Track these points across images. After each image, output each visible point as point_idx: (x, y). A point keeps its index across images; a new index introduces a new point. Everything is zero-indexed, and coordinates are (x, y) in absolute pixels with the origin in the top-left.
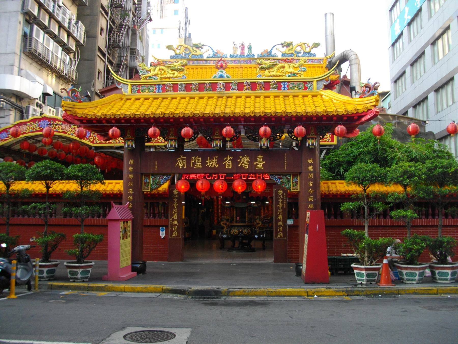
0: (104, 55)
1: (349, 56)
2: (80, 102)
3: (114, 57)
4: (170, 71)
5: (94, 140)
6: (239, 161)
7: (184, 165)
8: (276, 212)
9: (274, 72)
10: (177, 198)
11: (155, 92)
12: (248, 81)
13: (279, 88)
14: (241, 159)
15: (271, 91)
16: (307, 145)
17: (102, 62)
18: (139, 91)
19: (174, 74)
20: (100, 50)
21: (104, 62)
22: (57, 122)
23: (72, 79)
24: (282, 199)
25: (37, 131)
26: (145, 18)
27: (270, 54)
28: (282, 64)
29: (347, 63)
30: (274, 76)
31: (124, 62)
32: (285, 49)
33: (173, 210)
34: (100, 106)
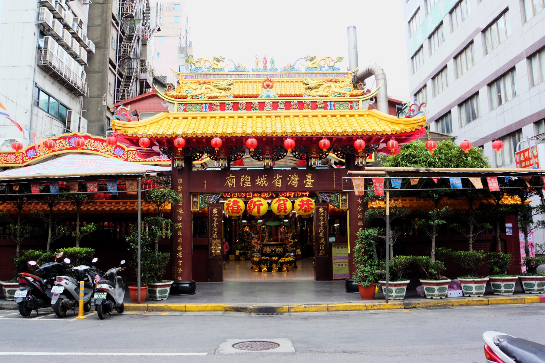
0: (114, 67)
1: (375, 71)
2: (130, 121)
3: (123, 69)
4: (217, 90)
5: (128, 158)
6: (288, 179)
7: (233, 184)
8: (318, 230)
9: (321, 91)
10: (216, 217)
11: (202, 111)
12: (295, 101)
13: (326, 108)
14: (290, 178)
15: (318, 110)
16: (356, 163)
17: (112, 75)
18: (185, 110)
19: (221, 92)
20: (111, 62)
21: (115, 74)
22: (89, 139)
23: (84, 92)
24: (323, 216)
25: (67, 149)
26: (154, 28)
27: (294, 68)
28: (328, 84)
29: (372, 78)
30: (320, 96)
31: (134, 74)
32: (309, 64)
33: (212, 230)
34: (148, 125)
